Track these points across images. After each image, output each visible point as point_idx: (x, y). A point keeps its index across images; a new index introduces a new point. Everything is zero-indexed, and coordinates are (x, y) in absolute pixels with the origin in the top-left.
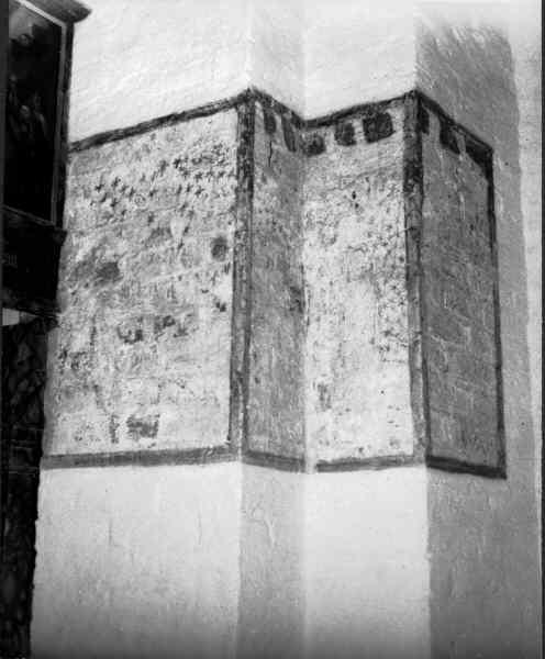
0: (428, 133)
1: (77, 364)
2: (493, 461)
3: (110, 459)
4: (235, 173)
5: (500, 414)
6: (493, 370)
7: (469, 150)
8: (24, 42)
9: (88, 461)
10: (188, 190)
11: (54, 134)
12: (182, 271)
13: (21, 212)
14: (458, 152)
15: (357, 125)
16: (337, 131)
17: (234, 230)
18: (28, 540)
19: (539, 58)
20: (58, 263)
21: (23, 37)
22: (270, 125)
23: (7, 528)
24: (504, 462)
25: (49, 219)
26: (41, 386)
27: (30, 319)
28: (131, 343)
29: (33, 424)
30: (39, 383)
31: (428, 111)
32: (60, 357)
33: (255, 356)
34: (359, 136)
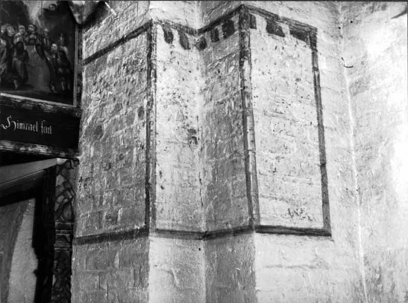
0: (256, 28)
1: (86, 185)
2: (319, 225)
3: (99, 238)
4: (147, 69)
5: (325, 194)
6: (318, 168)
7: (292, 33)
8: (51, 9)
9: (93, 239)
10: (129, 81)
11: (73, 58)
12: (190, 118)
13: (52, 103)
14: (283, 35)
15: (219, 28)
16: (212, 33)
17: (147, 101)
18: (67, 286)
19: (173, 2)
20: (79, 128)
21: (51, 6)
22: (169, 38)
23: (54, 280)
24: (329, 225)
25: (72, 104)
26: (72, 199)
27: (64, 162)
28: (107, 170)
29: (69, 221)
30: (71, 197)
31: (254, 15)
32: (80, 181)
33: (161, 173)
34: (221, 36)
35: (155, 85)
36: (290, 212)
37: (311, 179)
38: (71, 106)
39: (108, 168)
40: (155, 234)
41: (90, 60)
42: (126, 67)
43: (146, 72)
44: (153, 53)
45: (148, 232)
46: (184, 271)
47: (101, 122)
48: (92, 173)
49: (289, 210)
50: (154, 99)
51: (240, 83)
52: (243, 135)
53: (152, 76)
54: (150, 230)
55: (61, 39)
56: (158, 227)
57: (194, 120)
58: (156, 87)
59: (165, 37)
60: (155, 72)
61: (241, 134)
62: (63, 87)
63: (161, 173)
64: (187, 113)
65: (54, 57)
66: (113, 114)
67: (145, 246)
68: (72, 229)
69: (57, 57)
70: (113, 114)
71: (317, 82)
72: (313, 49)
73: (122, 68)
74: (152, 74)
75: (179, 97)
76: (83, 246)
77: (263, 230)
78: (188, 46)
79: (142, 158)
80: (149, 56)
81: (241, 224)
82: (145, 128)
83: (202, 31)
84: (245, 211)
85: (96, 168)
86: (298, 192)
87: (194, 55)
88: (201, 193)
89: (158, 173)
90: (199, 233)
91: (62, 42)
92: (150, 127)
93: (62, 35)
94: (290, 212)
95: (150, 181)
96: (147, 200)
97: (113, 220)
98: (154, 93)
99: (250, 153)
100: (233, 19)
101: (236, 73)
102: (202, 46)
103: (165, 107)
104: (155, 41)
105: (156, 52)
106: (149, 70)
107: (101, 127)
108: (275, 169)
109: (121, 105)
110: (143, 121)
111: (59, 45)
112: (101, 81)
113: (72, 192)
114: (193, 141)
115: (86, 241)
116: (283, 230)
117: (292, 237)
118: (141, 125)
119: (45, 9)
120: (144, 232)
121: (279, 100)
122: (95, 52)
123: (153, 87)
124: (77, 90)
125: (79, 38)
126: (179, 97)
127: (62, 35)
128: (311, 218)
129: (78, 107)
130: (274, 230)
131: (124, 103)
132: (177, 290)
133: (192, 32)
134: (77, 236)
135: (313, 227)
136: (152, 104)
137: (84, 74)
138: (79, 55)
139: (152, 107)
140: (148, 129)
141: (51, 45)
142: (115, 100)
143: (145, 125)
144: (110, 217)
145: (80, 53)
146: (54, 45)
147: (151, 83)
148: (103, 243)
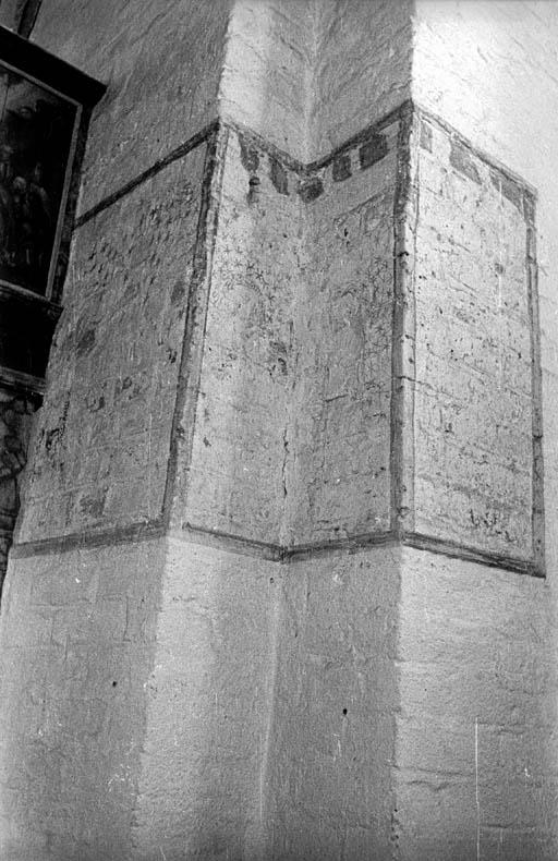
12: (275, 322)
15: (354, 154)
26: (18, 471)
30: (17, 466)
35: (214, 241)
36: (472, 517)
37: (514, 461)
38: (37, 296)
39: (96, 406)
40: (181, 533)
41: (87, 217)
42: (155, 216)
43: (197, 215)
44: (215, 178)
45: (167, 528)
46: (232, 620)
47: (94, 323)
48: (64, 419)
49: (471, 512)
50: (208, 266)
51: (392, 248)
52: (390, 350)
53: (208, 220)
54: (171, 524)
55: (36, 172)
56: (189, 518)
57: (284, 328)
58: (214, 244)
59: (241, 156)
60: (216, 215)
61: (387, 346)
62: (5, 201)
63: (206, 413)
64: (272, 311)
65: (17, 200)
66: (121, 304)
67: (158, 562)
68: (12, 529)
69: (22, 201)
70: (121, 304)
71: (533, 284)
72: (528, 223)
73: (149, 217)
74: (208, 217)
75: (259, 276)
76: (29, 559)
77: (418, 541)
78: (285, 189)
79: (171, 382)
80: (207, 182)
81: (371, 529)
82: (183, 322)
83: (314, 167)
84: (383, 504)
85: (73, 411)
86: (489, 481)
87: (295, 206)
88: (285, 469)
89: (200, 413)
90: (273, 547)
91: (38, 178)
92: (194, 317)
93: (39, 165)
94: (472, 517)
95: (182, 423)
96: (172, 463)
97: (95, 508)
98: (209, 254)
99: (406, 383)
100: (386, 131)
101: (383, 230)
102: (314, 192)
103: (229, 286)
104: (223, 158)
105: (221, 178)
106: (204, 210)
107: (93, 332)
108: (450, 426)
109: (139, 285)
110: (180, 308)
111: (29, 181)
112: (104, 249)
113: (21, 458)
114: (278, 365)
115: (36, 550)
116: (457, 551)
117: (470, 564)
118: (177, 315)
119: (9, 111)
120: (159, 528)
121: (92, 833)
122: (99, 201)
123: (209, 241)
124: (56, 272)
125: (72, 180)
126: (259, 276)
127: (39, 165)
128: (511, 536)
129: (57, 299)
130: (441, 548)
131: (144, 281)
132: (380, 532)
133: (296, 168)
134: (20, 542)
135: (513, 553)
136: (204, 274)
137: (73, 244)
138: (68, 210)
139: (202, 280)
140: (190, 322)
141: (13, 178)
142: (126, 278)
143: (185, 314)
144: (90, 502)
145: (71, 206)
146: (20, 179)
147: (204, 234)
148: (68, 554)
